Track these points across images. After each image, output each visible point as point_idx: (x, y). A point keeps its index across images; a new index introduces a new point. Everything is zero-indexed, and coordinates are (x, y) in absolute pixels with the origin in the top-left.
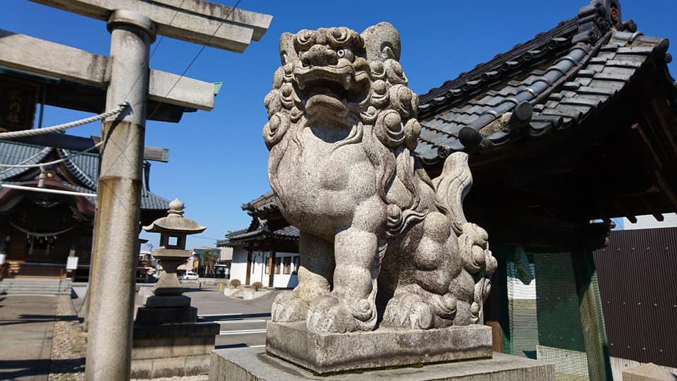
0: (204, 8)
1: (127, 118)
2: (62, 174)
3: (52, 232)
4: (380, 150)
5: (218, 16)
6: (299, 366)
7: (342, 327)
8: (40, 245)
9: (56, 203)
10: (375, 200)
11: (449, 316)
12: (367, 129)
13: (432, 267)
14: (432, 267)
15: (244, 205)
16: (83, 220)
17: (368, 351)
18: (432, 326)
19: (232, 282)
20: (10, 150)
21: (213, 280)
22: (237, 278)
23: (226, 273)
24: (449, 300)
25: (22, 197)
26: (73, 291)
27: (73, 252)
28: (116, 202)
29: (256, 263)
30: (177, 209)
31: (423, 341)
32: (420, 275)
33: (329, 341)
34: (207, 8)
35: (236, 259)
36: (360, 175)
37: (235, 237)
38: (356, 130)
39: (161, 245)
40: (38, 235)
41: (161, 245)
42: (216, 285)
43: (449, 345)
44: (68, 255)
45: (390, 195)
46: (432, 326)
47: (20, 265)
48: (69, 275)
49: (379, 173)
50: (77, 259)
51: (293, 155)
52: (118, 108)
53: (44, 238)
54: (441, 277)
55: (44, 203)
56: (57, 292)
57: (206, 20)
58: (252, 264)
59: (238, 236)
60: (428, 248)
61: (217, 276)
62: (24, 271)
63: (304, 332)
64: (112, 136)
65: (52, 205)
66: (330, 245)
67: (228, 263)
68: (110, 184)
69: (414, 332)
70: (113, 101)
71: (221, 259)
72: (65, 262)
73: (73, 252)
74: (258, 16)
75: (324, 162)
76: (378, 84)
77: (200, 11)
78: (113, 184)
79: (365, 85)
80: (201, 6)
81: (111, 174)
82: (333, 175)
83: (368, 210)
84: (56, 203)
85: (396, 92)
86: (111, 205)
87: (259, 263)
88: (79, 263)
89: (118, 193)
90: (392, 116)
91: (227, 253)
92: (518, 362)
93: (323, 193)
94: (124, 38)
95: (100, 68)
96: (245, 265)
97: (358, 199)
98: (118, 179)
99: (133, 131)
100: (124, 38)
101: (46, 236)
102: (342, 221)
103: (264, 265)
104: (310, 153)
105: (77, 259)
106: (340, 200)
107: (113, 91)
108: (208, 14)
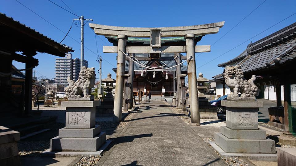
0: (206, 26)
1: (192, 59)
2: (157, 63)
3: (157, 81)
4: (238, 79)
5: (210, 27)
7: (234, 97)
8: (154, 86)
10: (238, 84)
11: (249, 96)
12: (236, 77)
13: (246, 91)
14: (246, 91)
15: (219, 65)
17: (237, 99)
18: (246, 97)
19: (218, 96)
21: (209, 96)
22: (220, 94)
23: (214, 92)
24: (249, 95)
26: (165, 99)
28: (192, 78)
29: (227, 89)
30: (201, 75)
31: (245, 99)
32: (245, 92)
33: (233, 98)
34: (207, 26)
35: (218, 87)
36: (235, 82)
37: (217, 79)
38: (235, 78)
39: (37, 54)
40: (153, 83)
41: (37, 54)
42: (210, 97)
43: (248, 99)
44: (162, 88)
45: (240, 84)
46: (246, 97)
48: (163, 94)
49: (238, 81)
50: (164, 89)
51: (228, 80)
52: (190, 58)
53: (155, 83)
54: (247, 92)
57: (207, 29)
58: (225, 89)
59: (218, 79)
60: (245, 89)
61: (211, 94)
63: (231, 98)
64: (189, 64)
66: (233, 89)
67: (215, 89)
68: (190, 74)
69: (243, 98)
70: (188, 56)
71: (212, 87)
72: (162, 90)
73: (163, 87)
74: (220, 23)
75: (231, 81)
76: (237, 72)
77: (205, 28)
78: (191, 75)
79: (235, 73)
80: (205, 26)
81: (190, 72)
82: (232, 83)
83: (237, 86)
85: (240, 73)
86: (191, 79)
87: (228, 88)
89: (192, 76)
90: (239, 75)
91: (214, 85)
93: (231, 84)
94: (189, 41)
95: (185, 49)
96: (222, 89)
97: (236, 85)
98: (192, 73)
99: (193, 61)
100: (189, 41)
102: (234, 87)
104: (230, 80)
105: (164, 89)
106: (233, 85)
107: (188, 54)
108: (207, 27)
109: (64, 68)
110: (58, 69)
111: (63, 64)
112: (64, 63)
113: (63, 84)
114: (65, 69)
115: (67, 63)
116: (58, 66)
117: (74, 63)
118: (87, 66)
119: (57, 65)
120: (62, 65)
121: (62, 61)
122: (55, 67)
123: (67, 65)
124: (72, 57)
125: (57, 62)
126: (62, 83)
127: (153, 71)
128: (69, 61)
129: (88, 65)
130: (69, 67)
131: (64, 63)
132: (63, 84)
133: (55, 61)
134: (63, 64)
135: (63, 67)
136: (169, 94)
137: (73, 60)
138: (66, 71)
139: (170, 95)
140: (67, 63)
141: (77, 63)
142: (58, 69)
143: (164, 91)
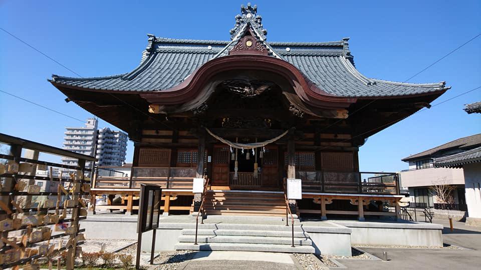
6: (249, 205)
8: (246, 165)
9: (263, 88)
16: (306, 114)
20: (202, 59)
25: (216, 83)
27: (292, 170)
40: (243, 147)
47: (226, 194)
53: (250, 151)
55: (246, 90)
56: (289, 248)
62: (232, 203)
65: (258, 92)
72: (283, 187)
84: (263, 88)
88: (304, 189)
92: (64, 161)
101: (253, 147)
103: (414, 197)
109: (79, 146)
110: (70, 138)
111: (79, 138)
112: (81, 136)
113: (78, 148)
114: (82, 147)
115: (86, 136)
116: (69, 142)
117: (100, 136)
118: (125, 147)
119: (67, 140)
120: (77, 141)
121: (77, 133)
122: (64, 143)
123: (86, 141)
124: (96, 126)
125: (67, 144)
126: (78, 147)
127: (242, 150)
128: (91, 133)
129: (126, 156)
130: (90, 143)
131: (81, 136)
132: (78, 148)
133: (65, 133)
134: (79, 138)
135: (78, 143)
136: (318, 207)
137: (99, 130)
138: (84, 146)
139: (324, 211)
140: (86, 136)
141: (105, 136)
142: (70, 138)
143: (294, 189)
